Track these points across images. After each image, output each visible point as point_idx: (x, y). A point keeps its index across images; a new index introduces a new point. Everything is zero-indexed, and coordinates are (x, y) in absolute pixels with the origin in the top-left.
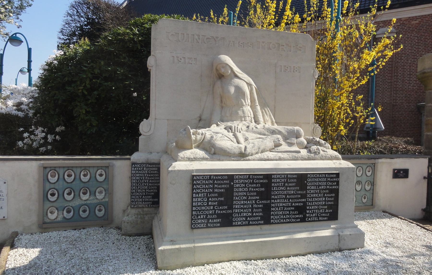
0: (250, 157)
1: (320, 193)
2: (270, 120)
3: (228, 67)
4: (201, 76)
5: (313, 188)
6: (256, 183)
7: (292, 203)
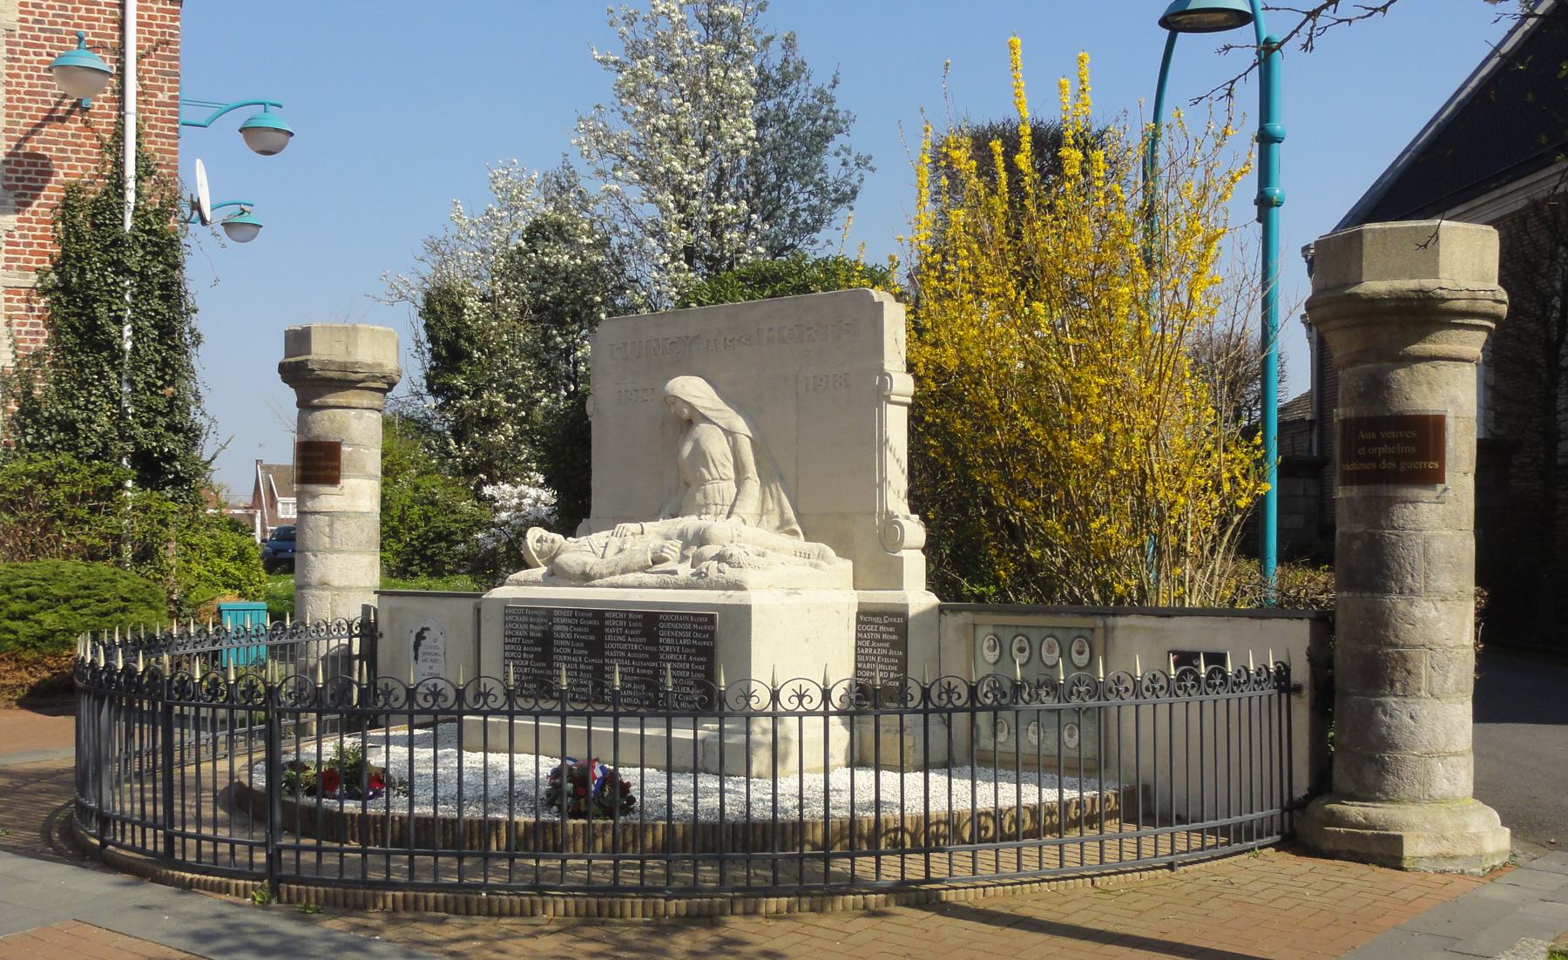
0: (597, 582)
1: (681, 653)
2: (777, 509)
3: (679, 403)
4: (663, 424)
5: (668, 641)
6: (583, 626)
7: (636, 667)
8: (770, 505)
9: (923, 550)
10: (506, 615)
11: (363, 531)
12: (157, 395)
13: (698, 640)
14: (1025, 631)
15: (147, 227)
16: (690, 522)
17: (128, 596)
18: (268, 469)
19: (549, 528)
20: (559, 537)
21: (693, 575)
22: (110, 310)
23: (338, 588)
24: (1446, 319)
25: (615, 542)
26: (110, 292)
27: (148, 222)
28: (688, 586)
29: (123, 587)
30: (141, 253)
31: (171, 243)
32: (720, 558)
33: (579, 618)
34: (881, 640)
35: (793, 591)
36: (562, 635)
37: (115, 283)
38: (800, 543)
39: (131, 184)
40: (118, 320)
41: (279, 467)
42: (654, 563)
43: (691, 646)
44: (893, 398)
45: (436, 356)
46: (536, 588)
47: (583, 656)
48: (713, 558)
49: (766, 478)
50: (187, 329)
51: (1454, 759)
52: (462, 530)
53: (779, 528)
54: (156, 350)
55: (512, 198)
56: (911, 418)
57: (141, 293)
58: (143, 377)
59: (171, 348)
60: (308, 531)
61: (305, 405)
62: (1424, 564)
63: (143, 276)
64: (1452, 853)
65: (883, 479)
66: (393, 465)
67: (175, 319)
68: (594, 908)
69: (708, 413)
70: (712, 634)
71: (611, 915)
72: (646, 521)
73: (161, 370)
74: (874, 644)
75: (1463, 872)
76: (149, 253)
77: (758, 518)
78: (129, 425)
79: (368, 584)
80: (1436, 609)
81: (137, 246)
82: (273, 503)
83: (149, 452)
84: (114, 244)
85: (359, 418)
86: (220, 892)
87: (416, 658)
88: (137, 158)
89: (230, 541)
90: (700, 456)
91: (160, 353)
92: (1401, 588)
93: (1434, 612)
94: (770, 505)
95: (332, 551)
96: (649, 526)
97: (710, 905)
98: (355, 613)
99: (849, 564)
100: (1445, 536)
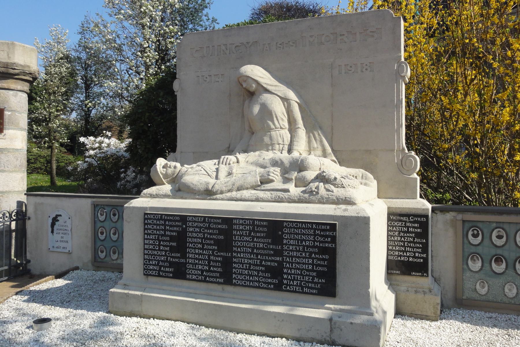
0: (218, 196)
2: (320, 148)
3: (250, 80)
10: (145, 219)
11: (17, 160)
13: (320, 242)
14: (501, 225)
28: (300, 201)
34: (408, 232)
36: (195, 235)
42: (262, 183)
43: (314, 247)
47: (213, 250)
49: (310, 129)
52: (34, 158)
69: (269, 88)
70: (334, 239)
74: (402, 234)
79: (21, 189)
85: (16, 96)
87: (52, 232)
94: (315, 144)
98: (13, 207)
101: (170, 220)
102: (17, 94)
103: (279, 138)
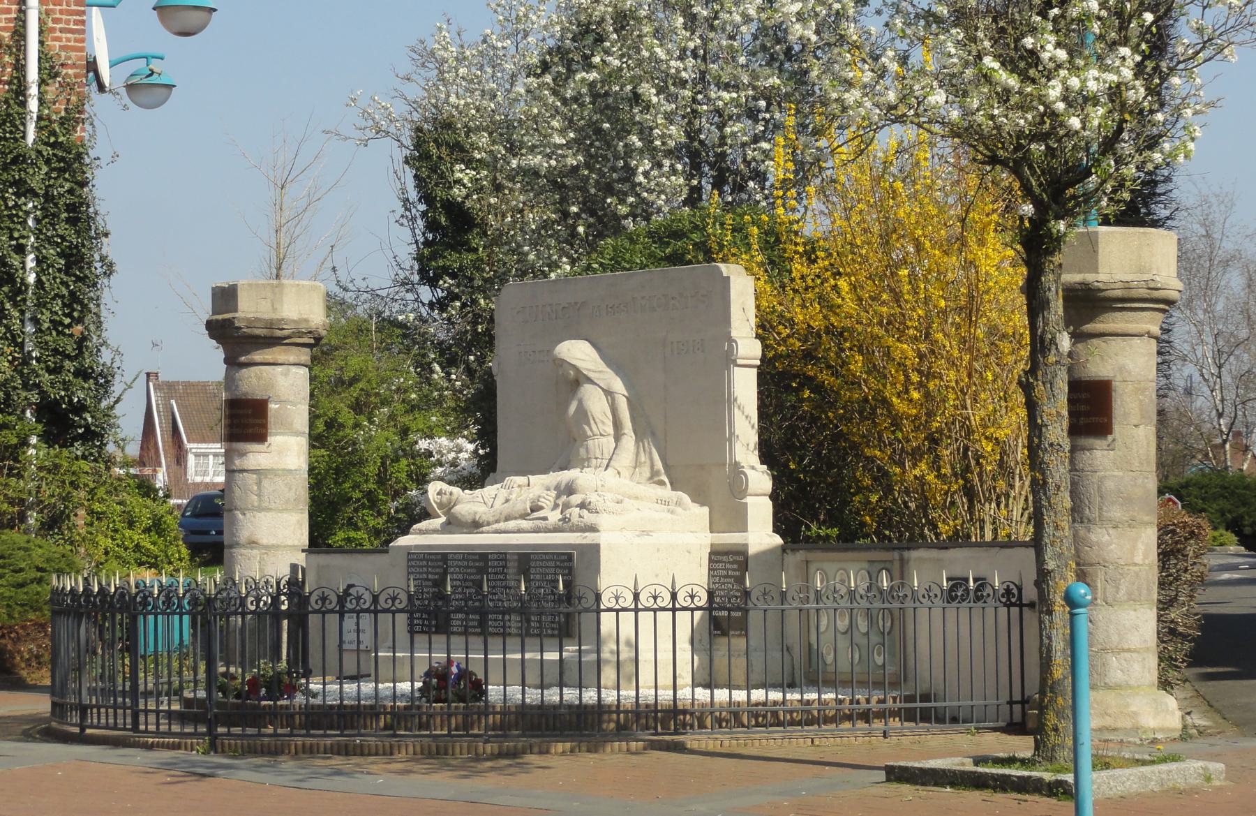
0: (485, 529)
2: (648, 462)
5: (538, 577)
6: (472, 567)
8: (643, 458)
9: (771, 497)
10: (409, 560)
11: (290, 489)
12: (64, 334)
15: (52, 140)
16: (565, 476)
17: (44, 565)
18: (169, 389)
19: (450, 483)
20: (456, 490)
21: (560, 520)
22: (12, 238)
23: (267, 547)
24: (1107, 304)
25: (503, 494)
26: (10, 217)
27: (53, 133)
28: (556, 530)
29: (38, 555)
30: (45, 169)
31: (79, 156)
32: (582, 506)
33: (468, 560)
35: (646, 533)
37: (16, 206)
38: (666, 492)
39: (33, 90)
40: (20, 250)
41: (188, 385)
42: (533, 511)
44: (739, 361)
45: (432, 226)
46: (435, 536)
48: (577, 506)
49: (639, 437)
50: (97, 257)
51: (1127, 655)
53: (651, 478)
54: (63, 283)
55: (518, 19)
56: (759, 375)
57: (44, 217)
58: (48, 314)
59: (79, 279)
60: (237, 490)
61: (233, 362)
62: (1098, 499)
63: (48, 198)
64: (1113, 726)
65: (732, 434)
66: (368, 395)
67: (83, 246)
68: (434, 749)
69: (591, 375)
71: (446, 754)
72: (533, 474)
73: (70, 306)
75: (1122, 740)
76: (52, 170)
77: (632, 469)
78: (34, 371)
79: (296, 543)
80: (1108, 534)
81: (41, 163)
82: (179, 457)
83: (57, 403)
84: (15, 161)
85: (286, 375)
86: (174, 749)
88: (40, 59)
89: (143, 510)
90: (583, 415)
91: (67, 286)
92: (1081, 518)
93: (1107, 537)
94: (643, 458)
95: (260, 509)
96: (536, 480)
97: (515, 747)
98: (284, 572)
99: (706, 510)
100: (1114, 476)
101: (432, 560)
102: (289, 370)
103: (597, 451)
